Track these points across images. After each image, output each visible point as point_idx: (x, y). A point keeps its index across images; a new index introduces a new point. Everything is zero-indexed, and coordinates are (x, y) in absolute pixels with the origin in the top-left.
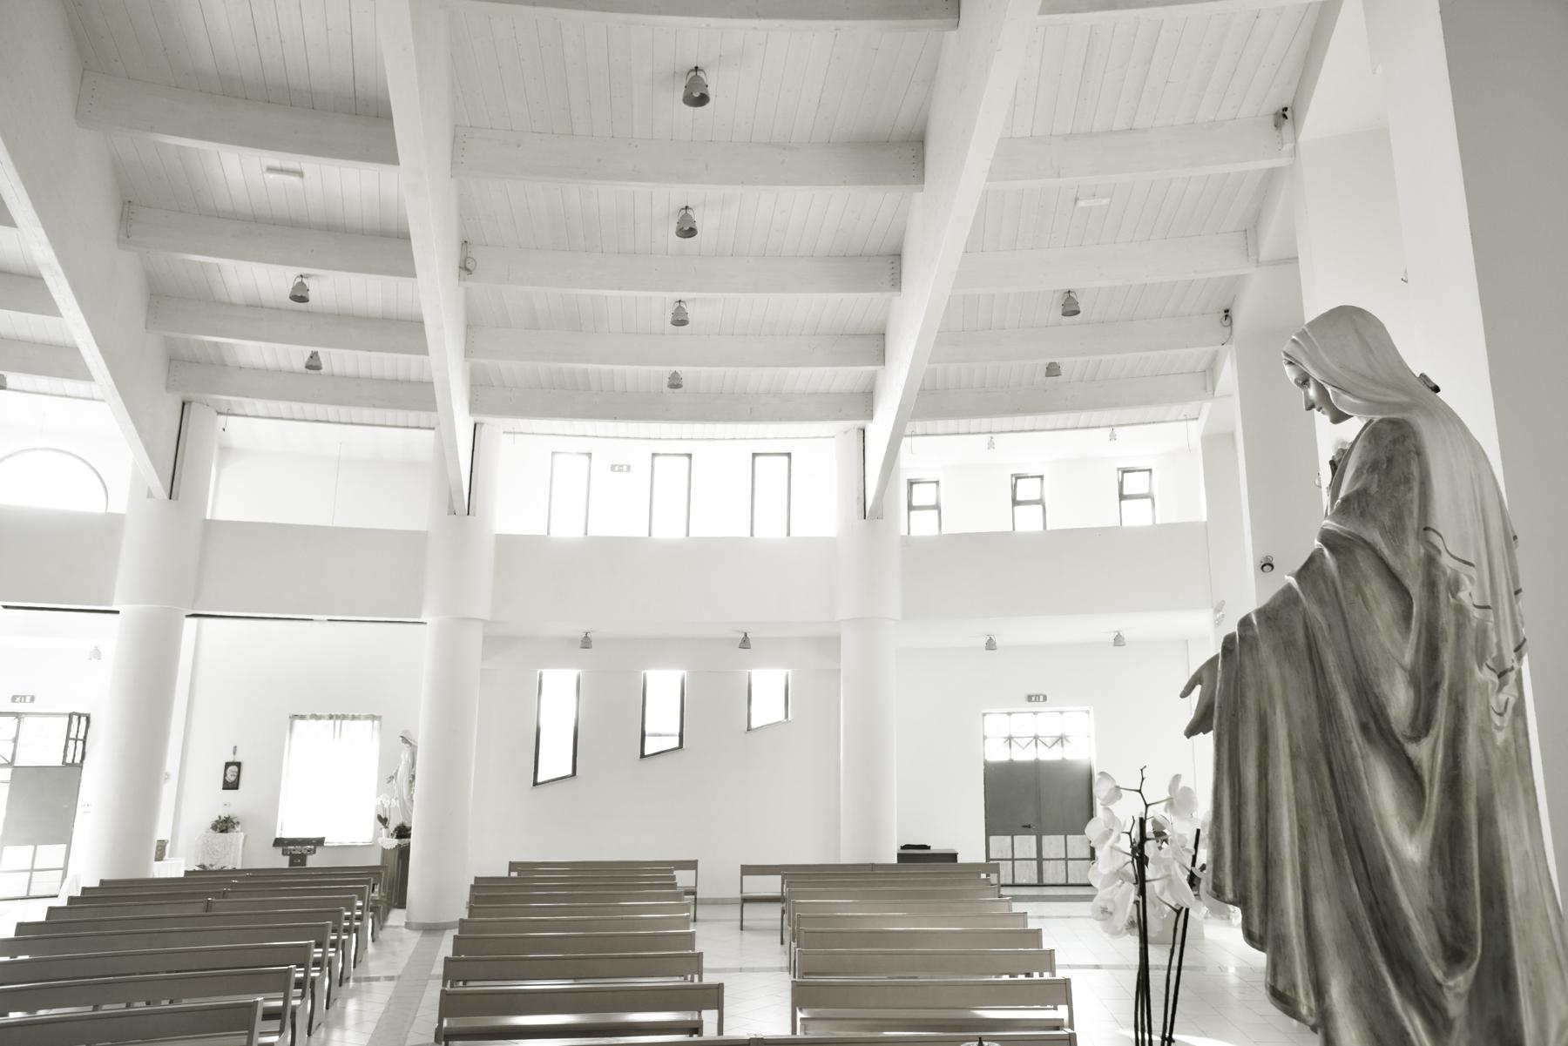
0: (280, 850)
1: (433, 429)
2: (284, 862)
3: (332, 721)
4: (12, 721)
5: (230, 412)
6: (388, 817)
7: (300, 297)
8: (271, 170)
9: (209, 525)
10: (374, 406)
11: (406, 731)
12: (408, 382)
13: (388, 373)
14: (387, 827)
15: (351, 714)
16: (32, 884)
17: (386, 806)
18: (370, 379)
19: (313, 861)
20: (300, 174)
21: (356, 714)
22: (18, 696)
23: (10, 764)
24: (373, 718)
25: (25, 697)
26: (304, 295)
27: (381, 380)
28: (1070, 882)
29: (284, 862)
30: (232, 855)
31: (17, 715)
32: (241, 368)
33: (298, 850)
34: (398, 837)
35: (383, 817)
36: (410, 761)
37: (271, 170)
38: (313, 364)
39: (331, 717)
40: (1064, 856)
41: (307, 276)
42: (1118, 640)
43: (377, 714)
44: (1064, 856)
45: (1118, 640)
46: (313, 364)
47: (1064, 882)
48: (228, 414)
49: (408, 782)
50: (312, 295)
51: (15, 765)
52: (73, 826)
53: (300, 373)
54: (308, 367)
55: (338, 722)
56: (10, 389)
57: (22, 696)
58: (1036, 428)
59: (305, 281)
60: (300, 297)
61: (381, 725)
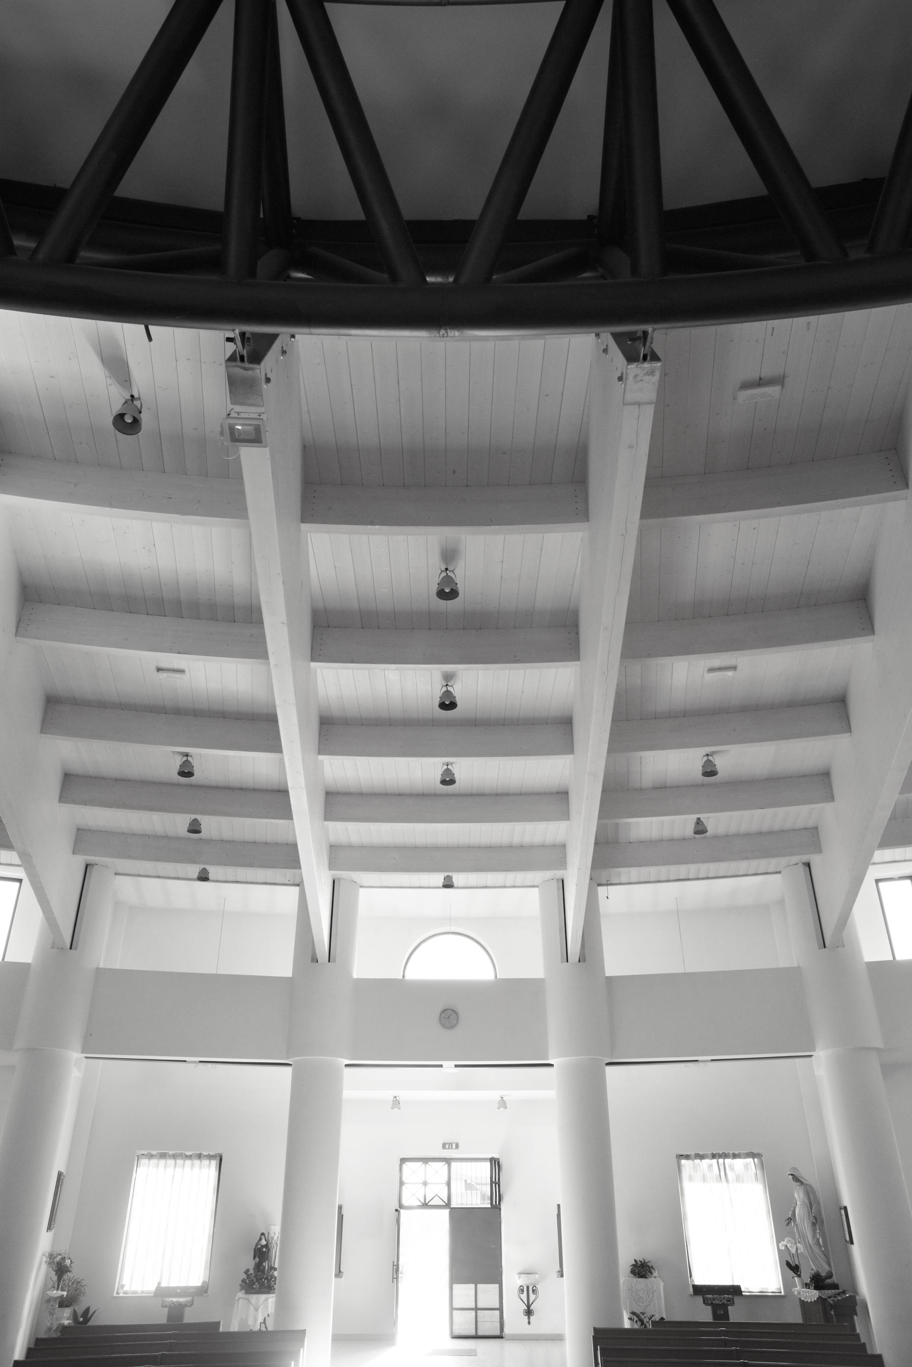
0: (700, 1299)
1: (780, 872)
2: (705, 1314)
3: (714, 1161)
4: (442, 1166)
5: (609, 882)
6: (797, 1263)
7: (710, 771)
8: (711, 670)
9: (610, 980)
10: (747, 858)
11: (794, 1169)
12: (771, 833)
13: (754, 827)
14: (799, 1276)
15: (731, 1152)
16: (479, 1323)
17: (793, 1251)
18: (737, 835)
19: (736, 1314)
20: (734, 668)
21: (736, 1152)
22: (447, 1144)
23: (448, 1205)
24: (752, 1155)
25: (452, 1144)
26: (713, 769)
27: (747, 835)
28: (480, 1333)
29: (705, 1314)
30: (656, 1301)
31: (448, 1161)
32: (630, 843)
33: (718, 1299)
34: (816, 1288)
35: (793, 1265)
36: (806, 1201)
37: (711, 670)
38: (700, 828)
39: (714, 1156)
40: (473, 1306)
41: (712, 754)
42: (396, 1102)
43: (755, 1152)
44: (473, 1306)
45: (396, 1102)
46: (700, 828)
47: (473, 1333)
48: (607, 885)
49: (810, 1225)
50: (719, 767)
51: (452, 1206)
52: (501, 1266)
53: (689, 839)
54: (696, 832)
55: (721, 1161)
56: (458, 888)
57: (449, 1144)
58: (907, 859)
59: (710, 758)
60: (710, 771)
61: (762, 1163)
